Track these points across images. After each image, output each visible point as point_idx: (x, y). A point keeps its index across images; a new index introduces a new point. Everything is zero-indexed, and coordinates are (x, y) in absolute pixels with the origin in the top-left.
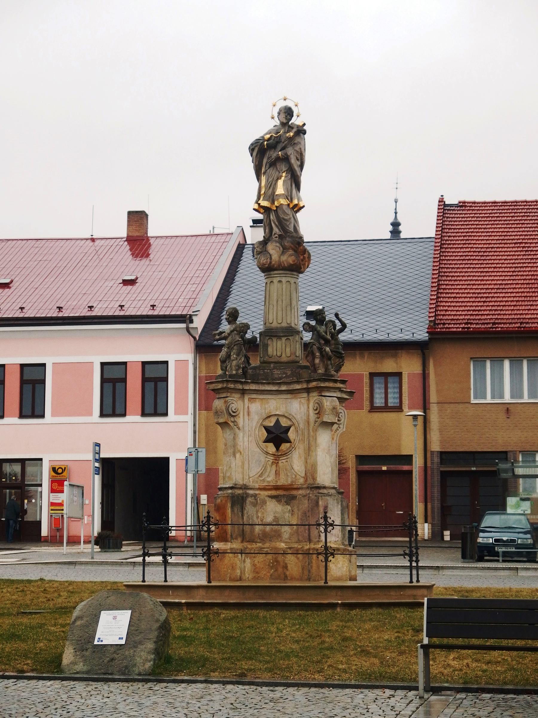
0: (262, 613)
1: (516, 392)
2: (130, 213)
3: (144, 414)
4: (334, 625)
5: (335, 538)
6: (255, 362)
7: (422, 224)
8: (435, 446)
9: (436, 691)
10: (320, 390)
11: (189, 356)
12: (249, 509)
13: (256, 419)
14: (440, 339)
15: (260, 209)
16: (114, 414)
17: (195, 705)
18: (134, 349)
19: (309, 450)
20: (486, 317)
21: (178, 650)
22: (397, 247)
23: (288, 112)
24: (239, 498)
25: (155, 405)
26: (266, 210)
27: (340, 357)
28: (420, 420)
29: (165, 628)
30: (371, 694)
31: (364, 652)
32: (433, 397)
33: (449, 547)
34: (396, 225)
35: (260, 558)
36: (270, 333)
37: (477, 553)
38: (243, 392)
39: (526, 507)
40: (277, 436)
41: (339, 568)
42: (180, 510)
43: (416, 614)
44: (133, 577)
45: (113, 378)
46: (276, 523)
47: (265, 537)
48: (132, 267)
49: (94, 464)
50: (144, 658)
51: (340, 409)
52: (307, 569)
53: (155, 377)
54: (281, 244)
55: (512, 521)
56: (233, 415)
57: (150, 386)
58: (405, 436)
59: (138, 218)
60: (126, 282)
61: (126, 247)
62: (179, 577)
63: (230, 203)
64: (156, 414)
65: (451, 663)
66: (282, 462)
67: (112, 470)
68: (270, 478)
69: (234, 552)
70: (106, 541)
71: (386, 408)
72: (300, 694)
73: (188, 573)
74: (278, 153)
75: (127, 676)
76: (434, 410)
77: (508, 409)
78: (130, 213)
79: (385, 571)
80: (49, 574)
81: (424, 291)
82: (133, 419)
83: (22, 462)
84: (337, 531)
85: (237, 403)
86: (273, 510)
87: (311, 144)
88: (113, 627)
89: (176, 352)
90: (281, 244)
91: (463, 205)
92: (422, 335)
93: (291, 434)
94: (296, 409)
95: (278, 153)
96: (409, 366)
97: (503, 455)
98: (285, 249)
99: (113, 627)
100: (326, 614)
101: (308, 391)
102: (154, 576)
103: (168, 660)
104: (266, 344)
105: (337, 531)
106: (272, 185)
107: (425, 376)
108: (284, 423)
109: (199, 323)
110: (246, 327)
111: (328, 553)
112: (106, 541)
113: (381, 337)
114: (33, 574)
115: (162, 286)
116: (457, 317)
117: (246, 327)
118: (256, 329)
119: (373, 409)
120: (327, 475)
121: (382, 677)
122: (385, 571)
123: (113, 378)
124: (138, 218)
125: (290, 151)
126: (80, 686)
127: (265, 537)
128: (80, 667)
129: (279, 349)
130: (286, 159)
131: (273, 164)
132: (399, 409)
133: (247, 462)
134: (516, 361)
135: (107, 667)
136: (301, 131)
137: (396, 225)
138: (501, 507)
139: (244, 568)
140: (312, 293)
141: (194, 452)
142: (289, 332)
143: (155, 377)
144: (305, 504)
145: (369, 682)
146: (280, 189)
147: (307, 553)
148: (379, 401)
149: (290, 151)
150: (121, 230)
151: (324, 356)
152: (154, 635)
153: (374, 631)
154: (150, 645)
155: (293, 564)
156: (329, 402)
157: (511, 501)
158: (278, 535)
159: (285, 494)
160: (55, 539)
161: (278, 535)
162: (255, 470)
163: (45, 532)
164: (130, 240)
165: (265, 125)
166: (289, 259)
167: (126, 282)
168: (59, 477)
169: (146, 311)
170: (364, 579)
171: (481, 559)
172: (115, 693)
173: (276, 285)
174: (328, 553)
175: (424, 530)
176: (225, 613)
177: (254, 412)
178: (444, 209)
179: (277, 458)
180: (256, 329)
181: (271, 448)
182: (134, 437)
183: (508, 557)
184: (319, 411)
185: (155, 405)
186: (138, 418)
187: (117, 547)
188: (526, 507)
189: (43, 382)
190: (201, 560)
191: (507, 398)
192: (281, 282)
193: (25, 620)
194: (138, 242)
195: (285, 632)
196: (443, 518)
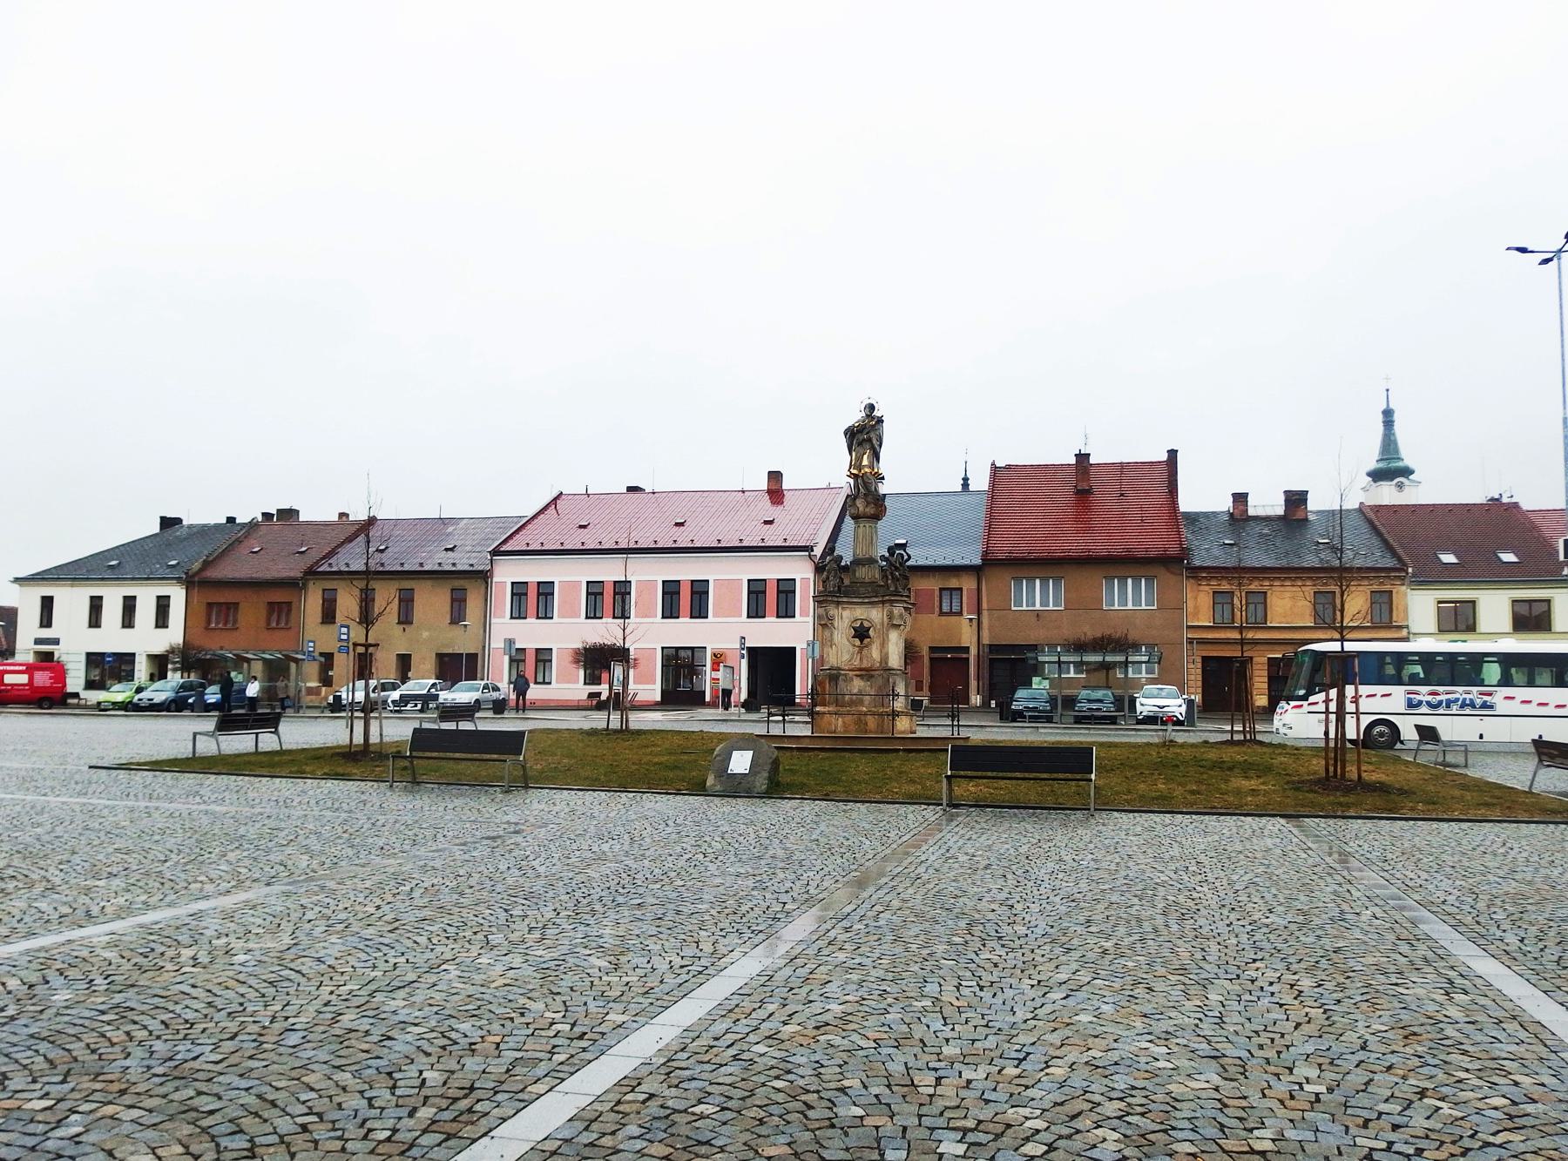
0: (847, 755)
1: (1044, 602)
2: (89, 655)
3: (778, 616)
4: (896, 764)
5: (899, 704)
6: (847, 582)
7: (980, 482)
8: (986, 641)
9: (956, 806)
10: (891, 602)
11: (811, 576)
12: (841, 683)
13: (846, 622)
14: (990, 564)
15: (851, 475)
16: (757, 616)
17: (792, 813)
18: (772, 569)
19: (883, 644)
20: (1023, 549)
21: (784, 778)
22: (966, 498)
23: (871, 407)
24: (835, 676)
25: (786, 610)
26: (855, 477)
27: (907, 578)
28: (975, 623)
29: (776, 764)
30: (911, 808)
31: (913, 781)
32: (985, 606)
33: (993, 711)
34: (966, 479)
35: (848, 719)
36: (857, 562)
37: (1009, 715)
38: (838, 603)
39: (1046, 684)
40: (861, 633)
41: (903, 724)
42: (802, 684)
43: (941, 756)
44: (760, 730)
45: (757, 590)
46: (860, 694)
47: (852, 703)
48: (769, 511)
49: (745, 741)
50: (761, 783)
51: (906, 615)
52: (881, 728)
53: (786, 590)
54: (866, 500)
55: (1036, 694)
56: (831, 619)
57: (456, 604)
58: (966, 634)
59: (775, 476)
60: (766, 522)
61: (767, 497)
62: (792, 730)
63: (824, 469)
64: (786, 616)
65: (967, 789)
66: (865, 651)
67: (758, 657)
68: (857, 663)
69: (830, 713)
70: (749, 706)
71: (951, 613)
72: (863, 807)
73: (799, 728)
74: (864, 436)
75: (749, 794)
76: (985, 614)
77: (1038, 614)
78: (89, 655)
79: (937, 728)
80: (707, 728)
81: (980, 531)
82: (684, 620)
83: (692, 649)
84: (902, 699)
85: (833, 611)
86: (857, 685)
87: (888, 430)
88: (741, 762)
89: (801, 572)
90: (866, 500)
91: (1008, 467)
92: (977, 561)
93: (871, 632)
94: (876, 615)
95: (864, 436)
96: (968, 584)
97: (1034, 648)
98: (868, 504)
99: (741, 762)
100: (891, 756)
101: (883, 602)
102: (776, 730)
103: (778, 784)
104: (864, 569)
105: (902, 699)
106: (860, 459)
107: (979, 590)
108: (866, 624)
109: (818, 551)
110: (841, 558)
111: (895, 714)
112: (749, 706)
113: (948, 562)
114: (696, 727)
115: (794, 524)
116: (1003, 548)
117: (841, 558)
118: (847, 560)
119: (942, 613)
120: (895, 659)
121: (920, 797)
122: (937, 728)
123: (757, 590)
124: (775, 476)
125: (872, 435)
126: (717, 800)
127: (852, 703)
128: (718, 788)
129: (863, 573)
130: (870, 440)
131: (860, 444)
132: (960, 613)
133: (842, 652)
134: (1137, 580)
135: (736, 788)
136: (880, 421)
137: (966, 479)
138: (1028, 684)
139: (838, 724)
140: (887, 533)
141: (811, 644)
142: (871, 561)
143: (786, 590)
144: (880, 681)
145: (912, 800)
146: (865, 462)
147: (881, 715)
148: (946, 608)
149: (872, 435)
150: (763, 484)
151: (896, 578)
152: (768, 767)
153: (920, 767)
154: (766, 775)
155: (872, 722)
156: (898, 610)
157: (1035, 680)
158: (861, 703)
159: (866, 673)
160: (713, 705)
161: (861, 703)
162: (846, 657)
163: (708, 699)
164: (769, 492)
165: (855, 416)
166: (870, 510)
167: (766, 522)
168: (718, 659)
169: (780, 543)
170: (922, 732)
171: (1014, 720)
172: (741, 807)
173: (861, 530)
174: (895, 714)
175: (976, 699)
176: (822, 755)
177: (845, 617)
178: (995, 469)
179: (861, 649)
180: (847, 560)
181: (857, 642)
182: (771, 633)
183: (1034, 719)
184: (891, 616)
185: (786, 611)
186: (774, 619)
187: (758, 710)
188: (1046, 684)
189: (707, 593)
190: (808, 719)
191: (1038, 607)
192: (865, 527)
193: (685, 757)
194: (775, 490)
195: (861, 767)
196: (990, 692)
